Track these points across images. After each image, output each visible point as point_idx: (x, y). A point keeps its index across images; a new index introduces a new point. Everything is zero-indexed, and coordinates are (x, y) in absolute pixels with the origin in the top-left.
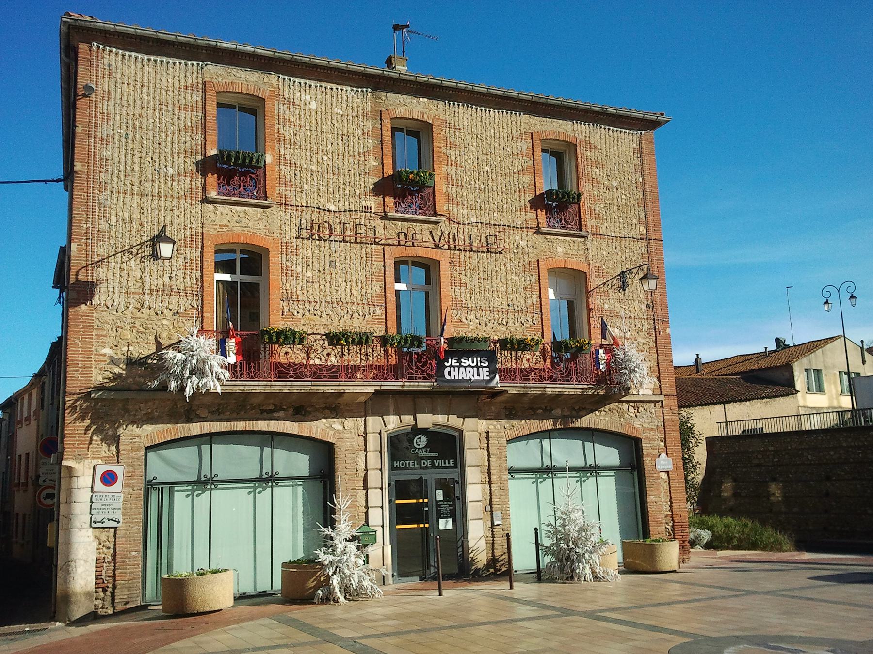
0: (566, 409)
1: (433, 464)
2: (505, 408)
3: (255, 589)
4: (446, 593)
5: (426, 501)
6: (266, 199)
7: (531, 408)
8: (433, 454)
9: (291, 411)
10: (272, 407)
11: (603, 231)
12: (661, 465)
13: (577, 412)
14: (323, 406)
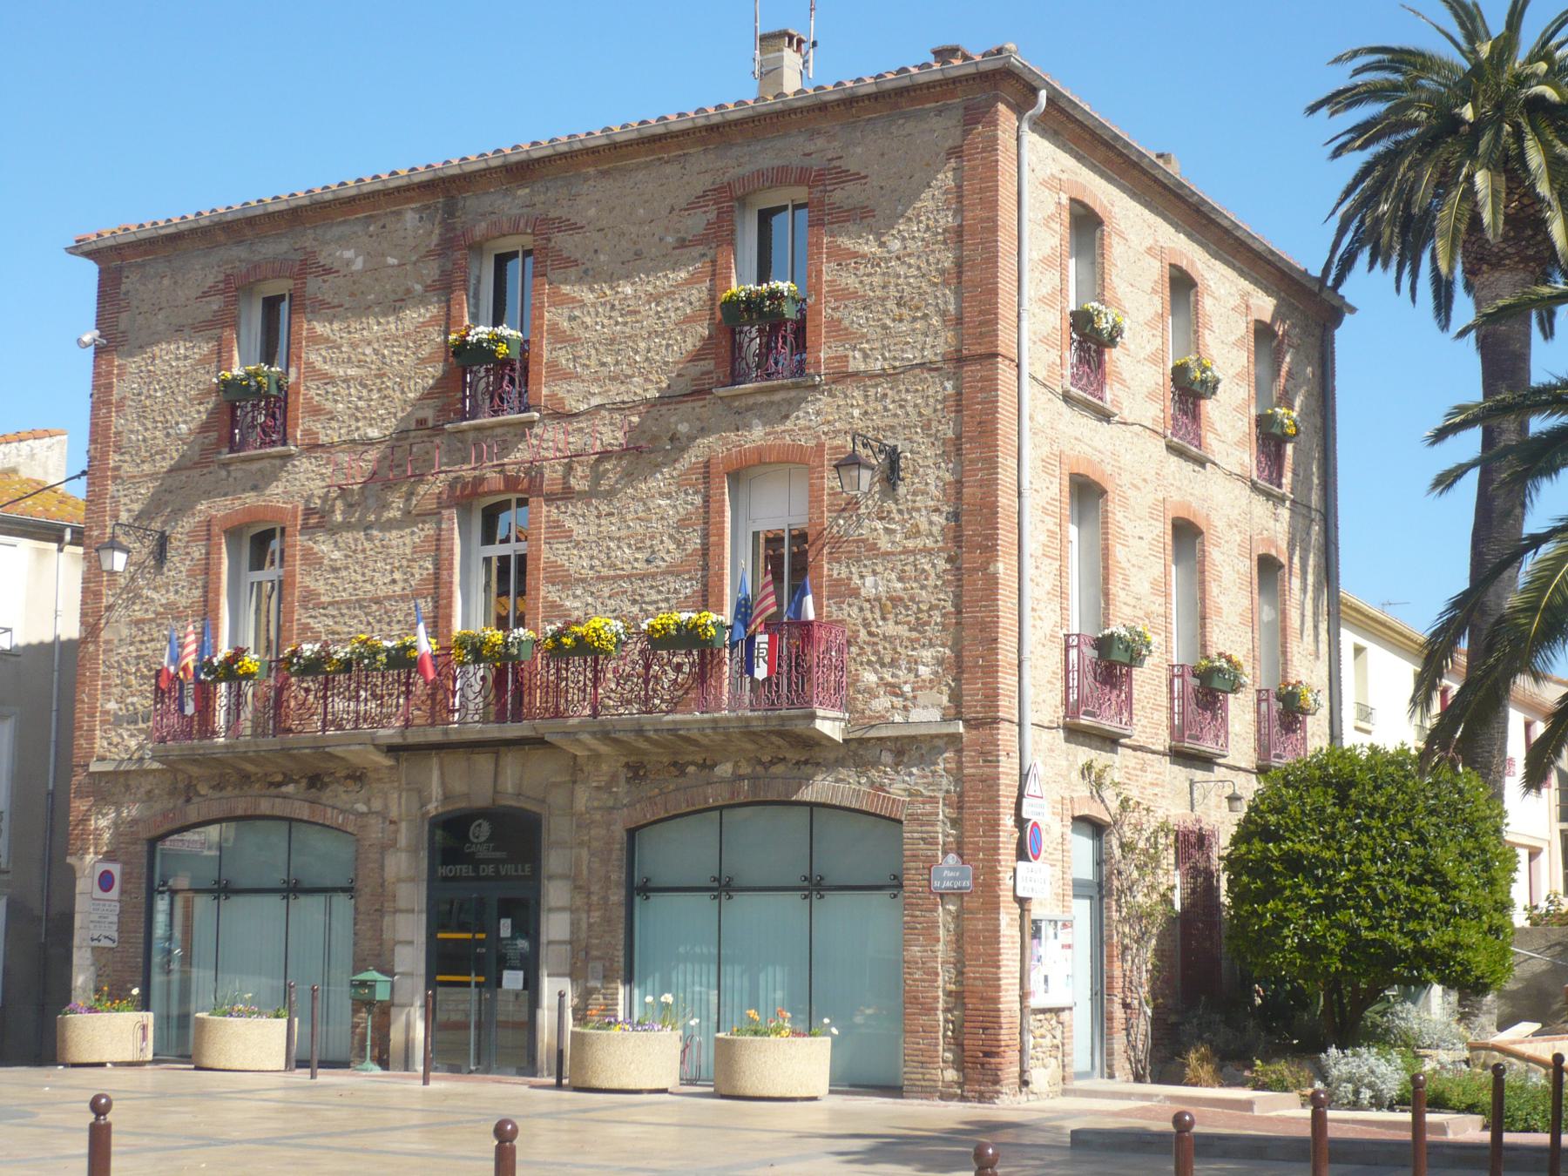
0: (743, 763)
1: (497, 871)
2: (627, 765)
3: (531, 1164)
4: (434, 1085)
5: (483, 936)
6: (285, 443)
7: (675, 764)
8: (498, 855)
9: (304, 782)
10: (279, 778)
11: (856, 363)
12: (942, 880)
13: (766, 769)
14: (344, 773)
